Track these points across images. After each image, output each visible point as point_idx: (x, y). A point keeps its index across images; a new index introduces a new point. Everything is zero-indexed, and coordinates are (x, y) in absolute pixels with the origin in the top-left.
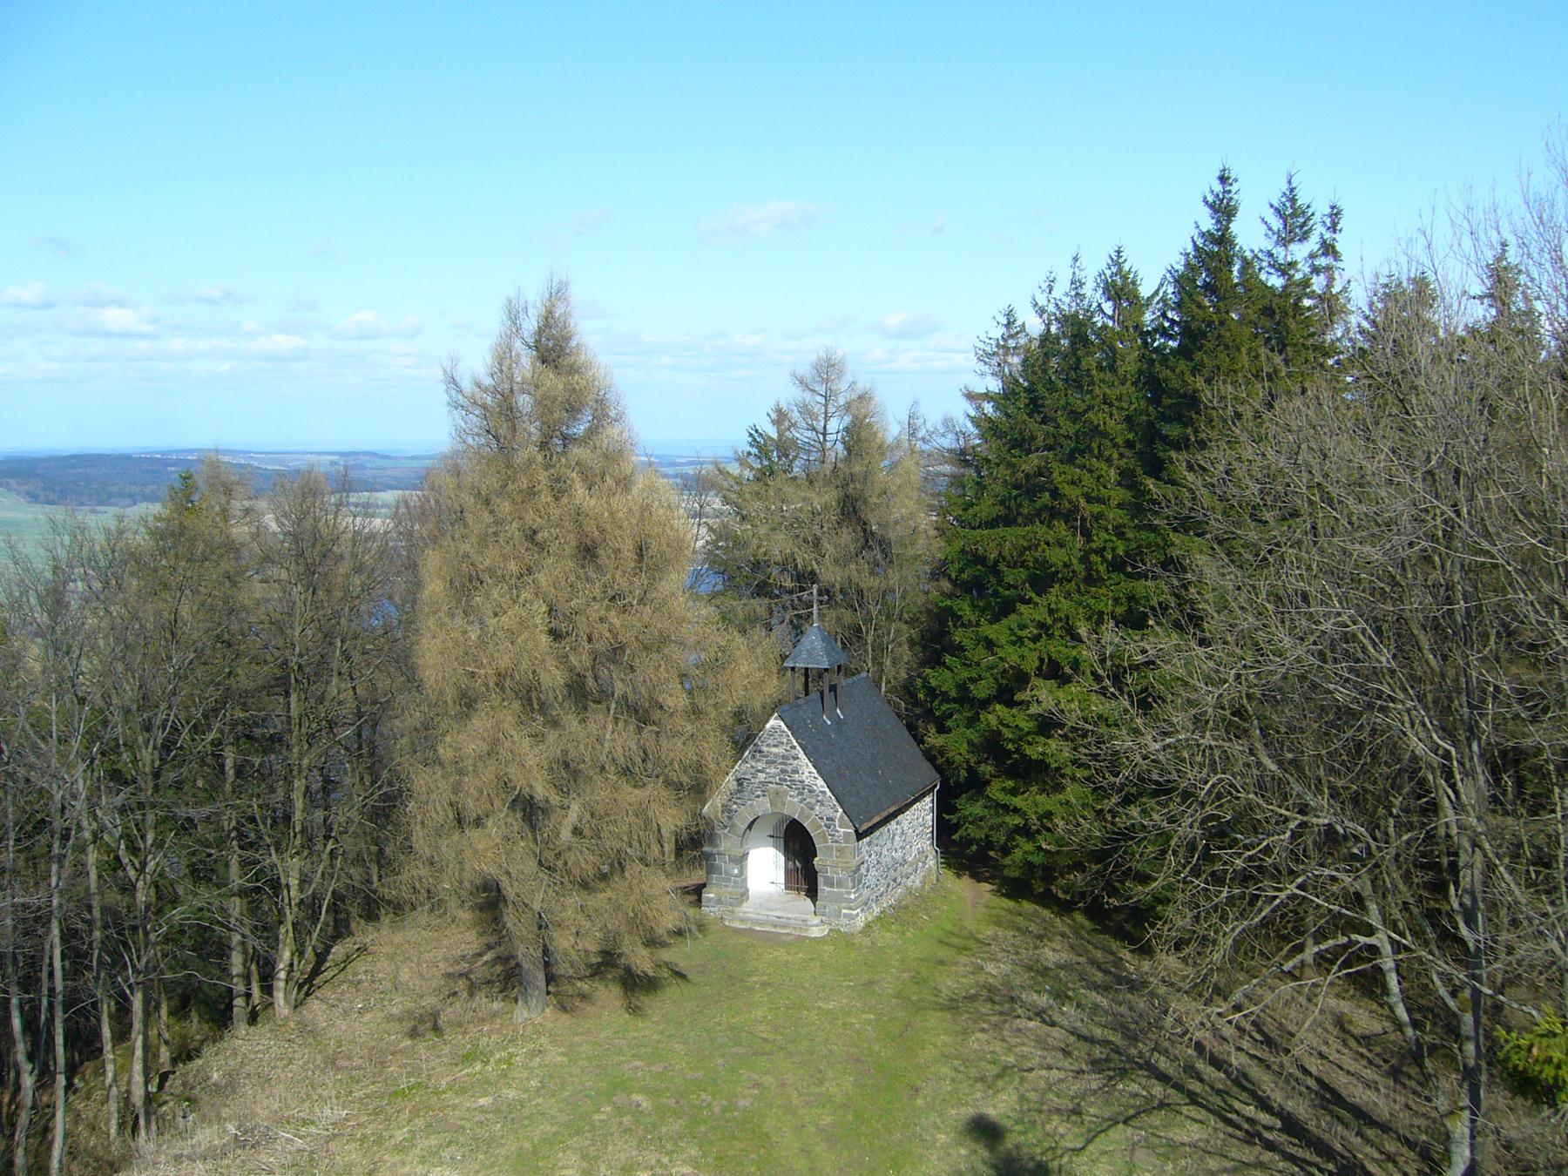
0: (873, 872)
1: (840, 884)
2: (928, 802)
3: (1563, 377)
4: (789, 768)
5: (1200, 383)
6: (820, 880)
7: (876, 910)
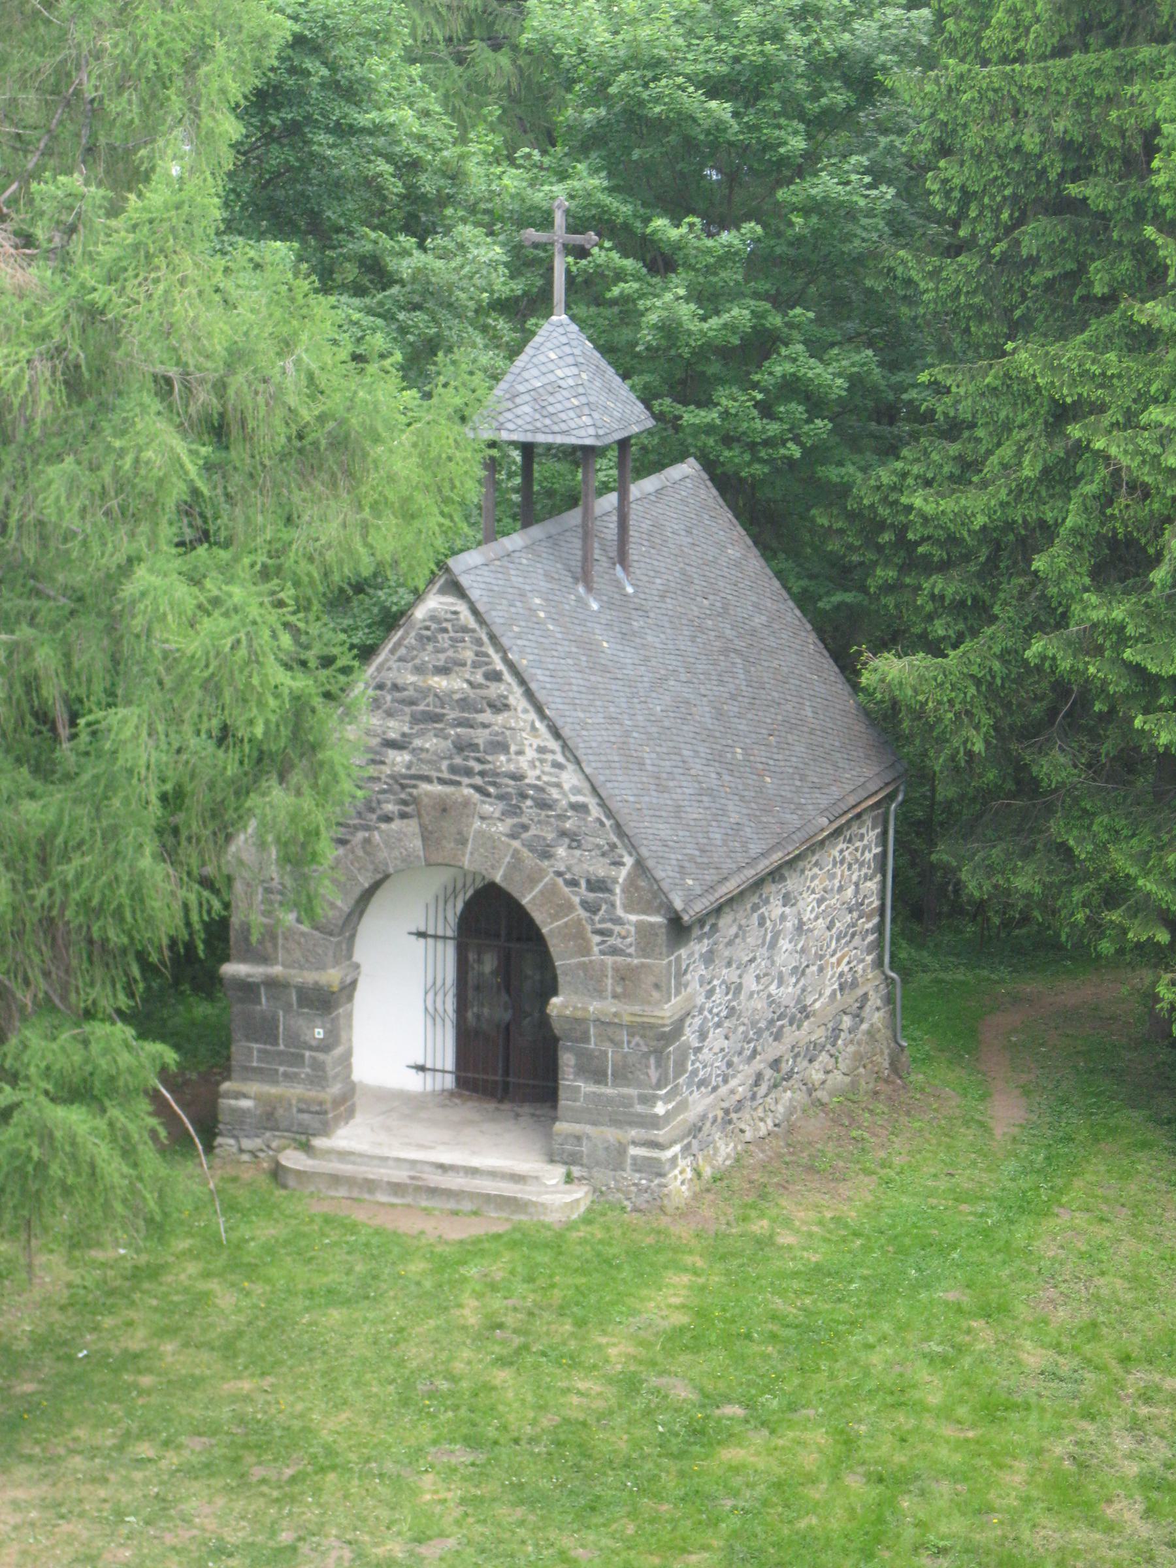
0: (716, 1039)
1: (622, 1075)
2: (867, 842)
3: (874, 1534)
4: (481, 737)
5: (273, 871)
6: (567, 1060)
7: (725, 1149)
